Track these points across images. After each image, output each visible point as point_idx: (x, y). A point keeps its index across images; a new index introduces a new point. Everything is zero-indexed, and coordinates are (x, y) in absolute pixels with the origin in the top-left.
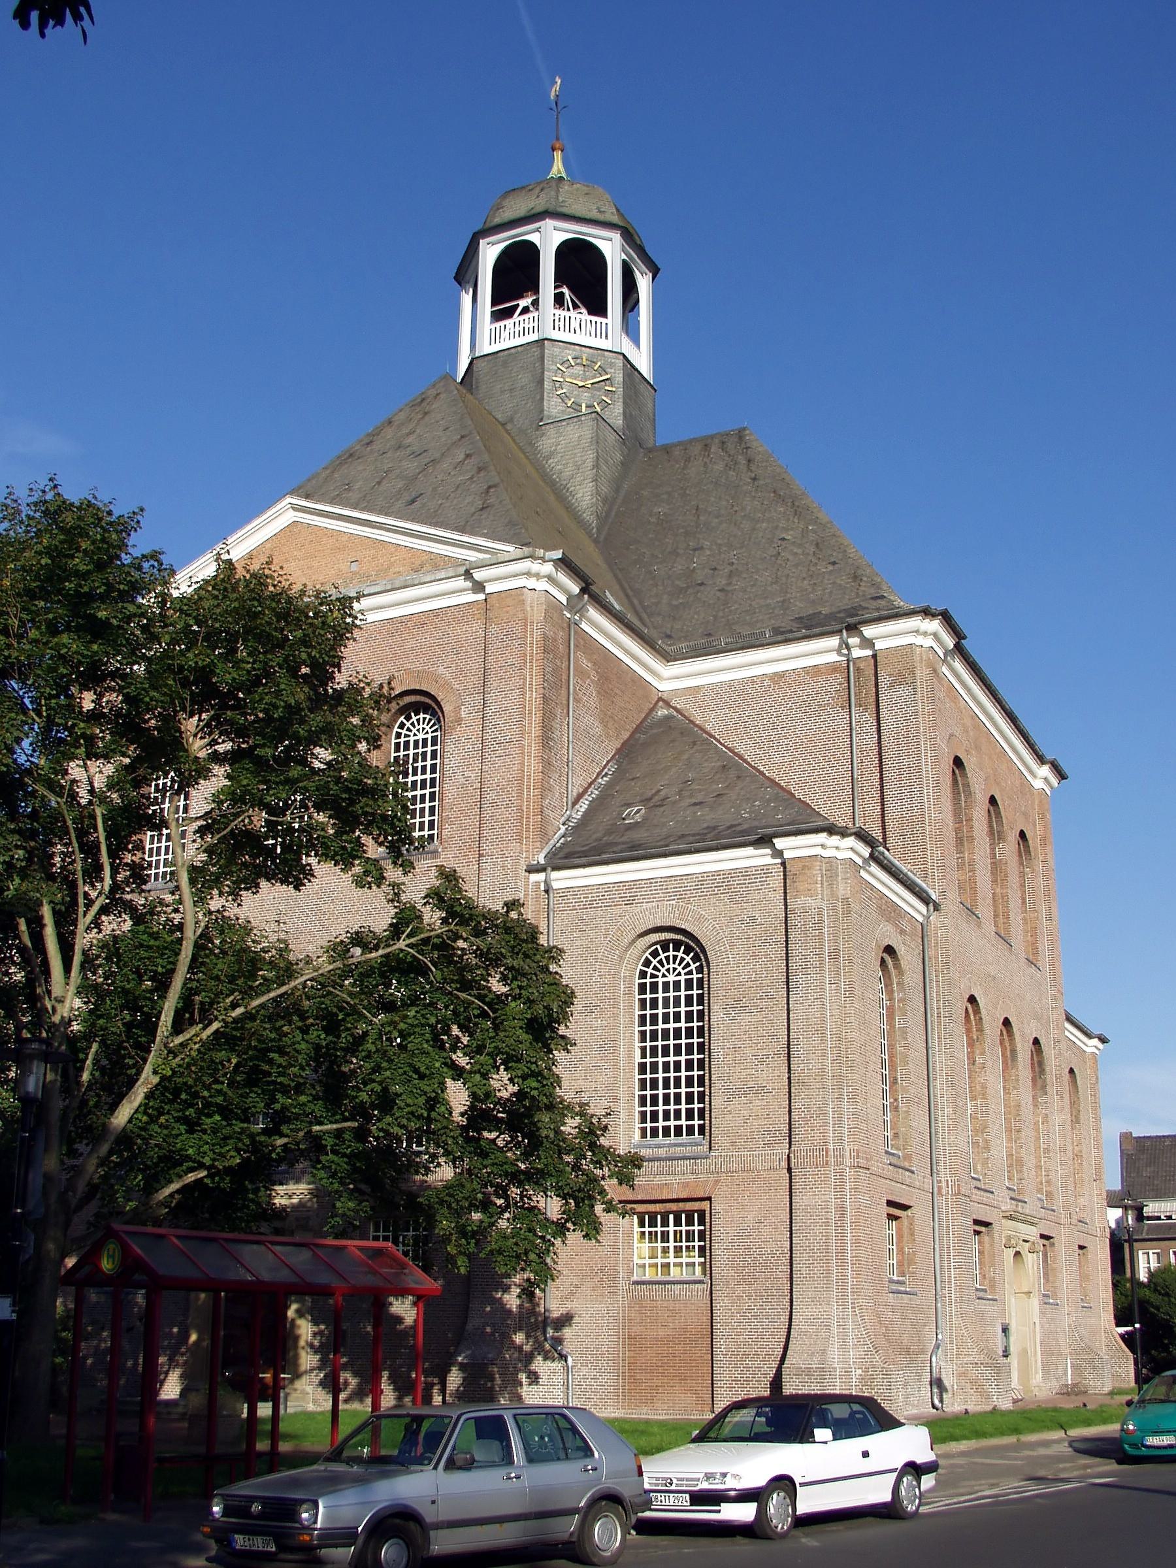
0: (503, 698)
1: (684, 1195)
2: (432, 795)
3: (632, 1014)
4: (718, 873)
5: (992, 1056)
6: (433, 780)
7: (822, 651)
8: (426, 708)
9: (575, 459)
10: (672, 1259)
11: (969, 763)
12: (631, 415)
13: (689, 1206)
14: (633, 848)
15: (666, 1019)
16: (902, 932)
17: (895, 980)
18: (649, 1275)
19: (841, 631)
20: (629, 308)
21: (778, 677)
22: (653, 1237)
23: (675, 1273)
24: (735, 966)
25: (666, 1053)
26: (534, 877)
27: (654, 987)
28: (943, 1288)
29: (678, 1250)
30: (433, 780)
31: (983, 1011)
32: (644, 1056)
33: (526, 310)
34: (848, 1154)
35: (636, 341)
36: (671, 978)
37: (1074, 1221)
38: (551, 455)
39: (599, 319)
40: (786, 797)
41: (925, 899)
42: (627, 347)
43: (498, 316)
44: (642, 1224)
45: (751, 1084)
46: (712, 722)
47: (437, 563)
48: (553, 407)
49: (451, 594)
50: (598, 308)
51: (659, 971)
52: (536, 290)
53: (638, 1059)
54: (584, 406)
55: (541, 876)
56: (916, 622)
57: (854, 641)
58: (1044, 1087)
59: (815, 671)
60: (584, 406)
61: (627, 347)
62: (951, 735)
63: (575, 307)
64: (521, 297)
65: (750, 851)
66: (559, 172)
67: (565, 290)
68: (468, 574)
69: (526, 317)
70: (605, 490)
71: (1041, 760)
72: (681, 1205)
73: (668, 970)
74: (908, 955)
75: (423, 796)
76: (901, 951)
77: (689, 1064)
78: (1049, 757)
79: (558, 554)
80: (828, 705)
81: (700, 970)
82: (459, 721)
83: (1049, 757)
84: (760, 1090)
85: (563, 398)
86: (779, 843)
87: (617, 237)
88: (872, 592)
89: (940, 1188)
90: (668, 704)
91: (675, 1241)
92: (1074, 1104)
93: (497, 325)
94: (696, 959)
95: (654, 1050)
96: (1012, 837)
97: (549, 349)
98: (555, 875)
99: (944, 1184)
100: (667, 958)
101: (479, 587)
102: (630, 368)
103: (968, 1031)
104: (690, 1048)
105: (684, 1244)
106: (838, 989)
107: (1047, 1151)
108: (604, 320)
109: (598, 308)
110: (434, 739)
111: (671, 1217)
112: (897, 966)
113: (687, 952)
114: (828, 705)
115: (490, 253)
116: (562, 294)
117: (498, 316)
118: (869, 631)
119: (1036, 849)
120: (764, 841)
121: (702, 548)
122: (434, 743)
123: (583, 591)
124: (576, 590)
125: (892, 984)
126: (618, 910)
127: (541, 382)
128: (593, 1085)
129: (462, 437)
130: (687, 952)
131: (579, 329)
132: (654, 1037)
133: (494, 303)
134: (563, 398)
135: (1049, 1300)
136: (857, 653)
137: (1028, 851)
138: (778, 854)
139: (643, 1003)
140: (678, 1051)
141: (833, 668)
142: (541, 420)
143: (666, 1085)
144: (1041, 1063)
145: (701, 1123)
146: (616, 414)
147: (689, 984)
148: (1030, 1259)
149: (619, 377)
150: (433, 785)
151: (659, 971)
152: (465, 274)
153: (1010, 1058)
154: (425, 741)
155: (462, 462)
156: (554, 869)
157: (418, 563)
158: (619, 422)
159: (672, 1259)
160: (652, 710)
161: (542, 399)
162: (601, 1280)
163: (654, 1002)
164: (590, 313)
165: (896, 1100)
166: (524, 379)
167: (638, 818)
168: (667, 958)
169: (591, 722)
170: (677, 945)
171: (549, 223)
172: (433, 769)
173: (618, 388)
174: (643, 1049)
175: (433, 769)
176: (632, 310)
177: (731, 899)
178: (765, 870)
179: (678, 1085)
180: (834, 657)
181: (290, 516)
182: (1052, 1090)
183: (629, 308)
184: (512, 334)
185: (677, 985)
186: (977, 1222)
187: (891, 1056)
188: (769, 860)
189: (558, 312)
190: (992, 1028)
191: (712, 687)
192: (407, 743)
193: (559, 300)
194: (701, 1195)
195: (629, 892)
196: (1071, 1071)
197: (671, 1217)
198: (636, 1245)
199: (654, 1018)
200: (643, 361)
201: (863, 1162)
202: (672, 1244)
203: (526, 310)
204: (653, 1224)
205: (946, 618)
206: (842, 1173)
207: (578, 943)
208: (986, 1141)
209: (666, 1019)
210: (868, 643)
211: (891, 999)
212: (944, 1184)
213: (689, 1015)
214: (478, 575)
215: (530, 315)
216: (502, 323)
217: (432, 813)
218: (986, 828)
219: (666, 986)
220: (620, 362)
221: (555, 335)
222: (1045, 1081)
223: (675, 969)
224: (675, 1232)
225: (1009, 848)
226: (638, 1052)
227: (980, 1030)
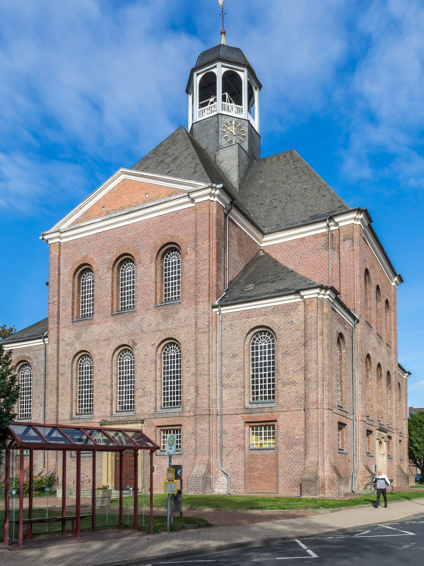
0: (204, 244)
1: (268, 420)
2: (179, 282)
3: (250, 358)
4: (279, 306)
5: (373, 375)
6: (179, 277)
7: (320, 228)
8: (176, 250)
9: (229, 161)
10: (263, 441)
11: (371, 272)
12: (251, 146)
13: (269, 423)
14: (250, 297)
15: (261, 359)
16: (345, 329)
17: (342, 346)
18: (255, 447)
19: (326, 220)
20: (251, 105)
21: (303, 239)
22: (257, 434)
23: (264, 446)
24: (287, 339)
25: (261, 371)
26: (215, 310)
27: (257, 348)
28: (356, 452)
29: (265, 438)
30: (179, 277)
31: (372, 360)
32: (253, 372)
33: (212, 103)
34: (325, 405)
35: (254, 118)
36: (263, 344)
37: (399, 432)
38: (221, 162)
39: (239, 106)
40: (305, 279)
41: (354, 318)
42: (250, 118)
43: (201, 106)
44: (253, 430)
45: (291, 381)
46: (278, 257)
47: (176, 192)
48: (223, 142)
49: (181, 204)
50: (239, 102)
51: (259, 342)
52: (215, 95)
53: (251, 373)
54: (234, 142)
55: (217, 310)
56: (354, 215)
57: (332, 224)
58: (390, 387)
59: (317, 236)
60: (234, 142)
61: (250, 118)
62: (365, 260)
63: (231, 102)
64: (210, 97)
65: (293, 297)
66: (224, 43)
67: (226, 94)
68: (188, 196)
69: (212, 105)
70: (242, 175)
71: (395, 274)
72: (266, 423)
73: (262, 342)
74: (347, 338)
75: (175, 282)
76: (345, 336)
77: (269, 375)
78: (398, 274)
79: (221, 186)
80: (321, 249)
81: (273, 341)
82: (187, 253)
83: (398, 274)
84: (294, 383)
85: (226, 138)
86: (302, 293)
87: (245, 70)
88: (339, 205)
89: (356, 419)
90: (263, 251)
91: (264, 435)
92: (400, 394)
93: (201, 109)
94: (272, 337)
95: (257, 370)
96: (384, 301)
97: (221, 118)
98: (222, 309)
99: (357, 417)
100: (262, 337)
101: (193, 200)
102: (251, 127)
103: (366, 366)
104: (269, 369)
105: (267, 436)
106: (323, 346)
107: (390, 409)
108: (241, 107)
109: (239, 102)
110: (179, 261)
111: (263, 427)
112: (344, 341)
113: (268, 335)
114: (321, 249)
115: (197, 79)
116: (225, 95)
117: (201, 106)
118: (337, 219)
119: (391, 306)
120: (297, 292)
121: (276, 194)
122: (179, 263)
123: (231, 203)
124: (228, 202)
125: (341, 348)
126: (244, 320)
127: (218, 132)
128: (236, 382)
129: (187, 148)
130: (268, 335)
131: (233, 110)
132: (257, 365)
133: (200, 100)
134: (226, 138)
135: (390, 457)
136: (332, 228)
137: (388, 307)
138: (302, 297)
139: (253, 354)
140: (265, 370)
141: (323, 234)
142: (218, 147)
143: (261, 382)
144: (389, 380)
145: (272, 396)
146: (246, 145)
147: (269, 346)
148: (384, 444)
149: (247, 130)
150: (179, 278)
151: (259, 342)
152: (189, 90)
153: (379, 376)
154: (175, 262)
155: (187, 157)
156: (222, 306)
157: (170, 193)
158: (246, 148)
159: (263, 441)
160: (257, 253)
161: (218, 139)
162: (239, 449)
163: (257, 353)
164: (235, 104)
165: (342, 388)
166: (212, 131)
167: (252, 288)
168: (262, 337)
169: (235, 256)
170: (265, 332)
171: (219, 64)
172: (179, 272)
173: (246, 134)
174: (253, 370)
175: (179, 272)
176: (252, 106)
177: (284, 315)
178: (297, 304)
179: (265, 382)
180: (325, 230)
181: (123, 176)
182: (393, 389)
183: (251, 105)
184: (207, 113)
185: (265, 347)
186: (367, 430)
187: (340, 373)
188: (300, 300)
189: (223, 103)
190: (374, 366)
191: (279, 244)
192: (169, 263)
193: (224, 99)
194: (273, 419)
195: (248, 314)
196: (399, 383)
197: (263, 427)
198: (251, 437)
199: (257, 359)
200: (256, 126)
201: (331, 408)
202: (263, 437)
203: (212, 103)
204: (257, 430)
205: (366, 213)
206: (323, 412)
207: (230, 333)
208: (372, 404)
209: (261, 359)
210: (337, 224)
211: (341, 352)
212: (357, 417)
213: (269, 358)
214: (192, 196)
215: (213, 104)
216: (203, 108)
217: (179, 288)
218: (375, 296)
219: (261, 347)
220: (247, 124)
221: (223, 112)
222: (391, 385)
223: (264, 341)
224: (264, 432)
225: (382, 304)
226: (251, 371)
227: (371, 366)
